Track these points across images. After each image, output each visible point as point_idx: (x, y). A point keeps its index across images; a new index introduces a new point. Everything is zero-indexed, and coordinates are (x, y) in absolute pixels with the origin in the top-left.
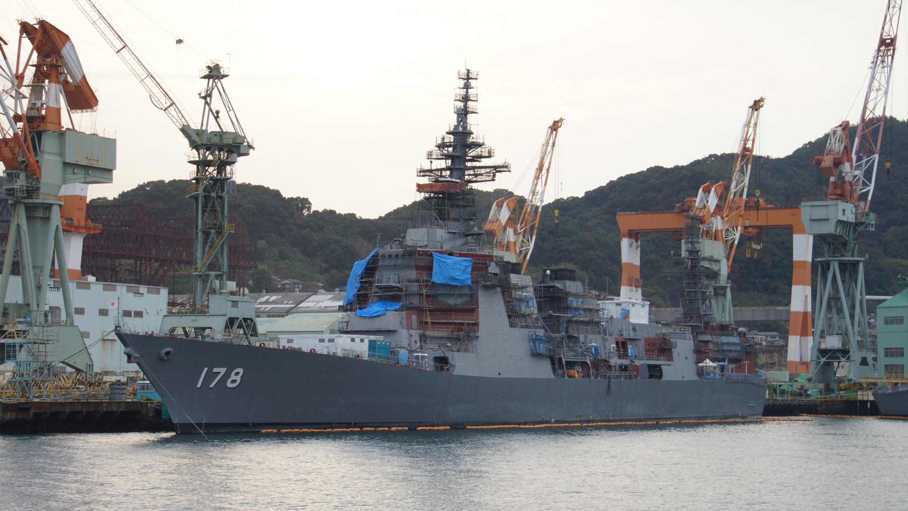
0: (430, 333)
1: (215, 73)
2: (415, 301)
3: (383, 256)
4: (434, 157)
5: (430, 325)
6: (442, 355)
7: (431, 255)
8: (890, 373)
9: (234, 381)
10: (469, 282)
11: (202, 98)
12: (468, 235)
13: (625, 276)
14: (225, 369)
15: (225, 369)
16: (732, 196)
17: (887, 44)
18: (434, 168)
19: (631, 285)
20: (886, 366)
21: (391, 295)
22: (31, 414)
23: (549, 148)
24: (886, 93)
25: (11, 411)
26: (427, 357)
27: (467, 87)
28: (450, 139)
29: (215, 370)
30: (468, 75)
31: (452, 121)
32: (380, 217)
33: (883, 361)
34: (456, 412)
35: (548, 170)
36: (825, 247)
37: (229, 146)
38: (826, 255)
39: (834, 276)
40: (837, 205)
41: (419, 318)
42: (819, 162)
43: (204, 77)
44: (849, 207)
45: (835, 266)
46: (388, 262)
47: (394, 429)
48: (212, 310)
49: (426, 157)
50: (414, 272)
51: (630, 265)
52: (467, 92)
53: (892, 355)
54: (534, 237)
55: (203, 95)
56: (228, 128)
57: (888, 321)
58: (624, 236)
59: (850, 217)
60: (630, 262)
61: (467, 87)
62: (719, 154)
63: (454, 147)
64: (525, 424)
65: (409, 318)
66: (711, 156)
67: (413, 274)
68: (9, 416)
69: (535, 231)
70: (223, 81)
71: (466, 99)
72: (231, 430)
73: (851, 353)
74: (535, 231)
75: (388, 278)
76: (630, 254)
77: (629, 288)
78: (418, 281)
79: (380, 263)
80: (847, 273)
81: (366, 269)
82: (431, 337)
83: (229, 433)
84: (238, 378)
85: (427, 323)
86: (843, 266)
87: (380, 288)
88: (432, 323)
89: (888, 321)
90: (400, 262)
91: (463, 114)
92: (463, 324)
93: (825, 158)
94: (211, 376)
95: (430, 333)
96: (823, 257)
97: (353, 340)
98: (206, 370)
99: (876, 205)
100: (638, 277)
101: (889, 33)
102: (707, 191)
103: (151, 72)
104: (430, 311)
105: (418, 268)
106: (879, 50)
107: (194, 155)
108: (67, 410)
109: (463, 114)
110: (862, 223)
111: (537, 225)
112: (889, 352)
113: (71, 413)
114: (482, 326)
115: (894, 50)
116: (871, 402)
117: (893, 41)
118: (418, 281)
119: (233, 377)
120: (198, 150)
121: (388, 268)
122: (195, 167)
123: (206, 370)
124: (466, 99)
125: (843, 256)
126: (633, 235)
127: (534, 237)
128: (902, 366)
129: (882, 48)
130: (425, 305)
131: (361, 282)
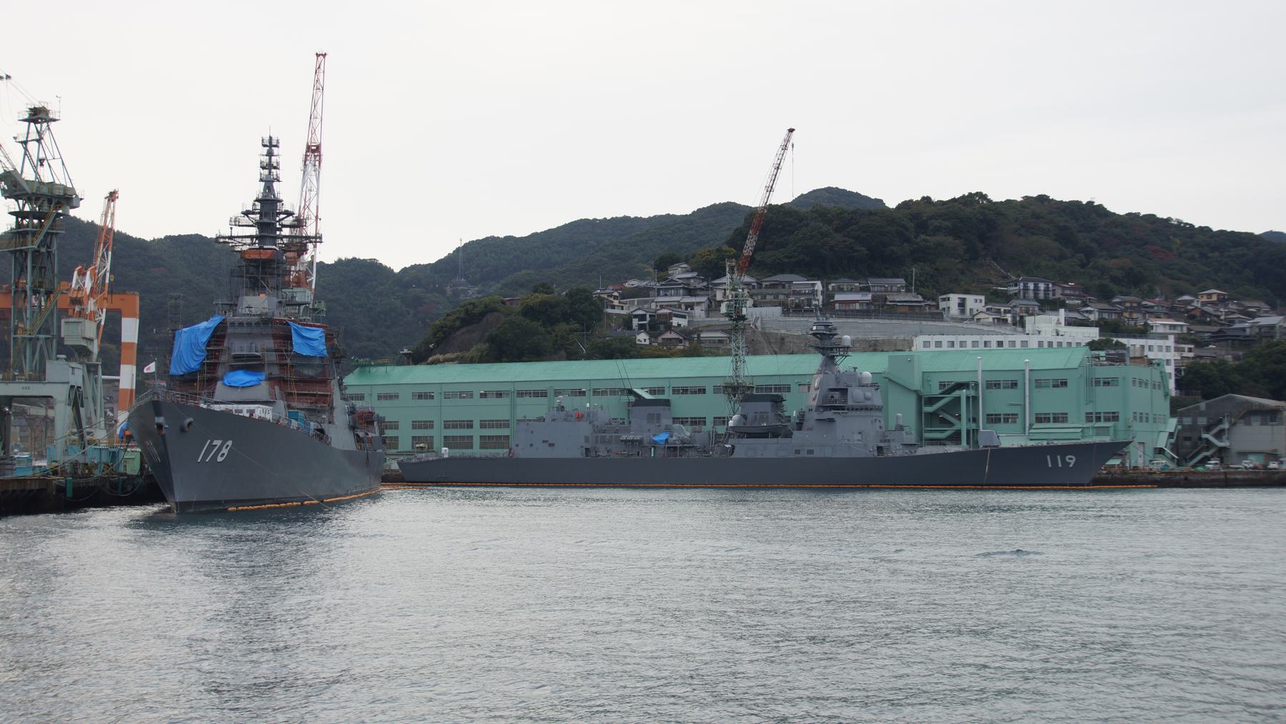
2: (276, 371)
3: (233, 324)
13: (125, 353)
18: (234, 234)
21: (250, 364)
27: (270, 154)
28: (258, 206)
37: (59, 197)
46: (239, 330)
48: (49, 376)
56: (61, 180)
61: (270, 154)
67: (270, 343)
70: (52, 125)
71: (269, 166)
75: (239, 347)
78: (276, 351)
79: (230, 330)
81: (213, 336)
83: (208, 512)
85: (291, 394)
87: (237, 357)
91: (269, 183)
94: (212, 446)
102: (82, 274)
105: (275, 337)
107: (13, 205)
109: (269, 183)
117: (318, 148)
119: (225, 451)
122: (14, 218)
124: (269, 166)
130: (287, 376)
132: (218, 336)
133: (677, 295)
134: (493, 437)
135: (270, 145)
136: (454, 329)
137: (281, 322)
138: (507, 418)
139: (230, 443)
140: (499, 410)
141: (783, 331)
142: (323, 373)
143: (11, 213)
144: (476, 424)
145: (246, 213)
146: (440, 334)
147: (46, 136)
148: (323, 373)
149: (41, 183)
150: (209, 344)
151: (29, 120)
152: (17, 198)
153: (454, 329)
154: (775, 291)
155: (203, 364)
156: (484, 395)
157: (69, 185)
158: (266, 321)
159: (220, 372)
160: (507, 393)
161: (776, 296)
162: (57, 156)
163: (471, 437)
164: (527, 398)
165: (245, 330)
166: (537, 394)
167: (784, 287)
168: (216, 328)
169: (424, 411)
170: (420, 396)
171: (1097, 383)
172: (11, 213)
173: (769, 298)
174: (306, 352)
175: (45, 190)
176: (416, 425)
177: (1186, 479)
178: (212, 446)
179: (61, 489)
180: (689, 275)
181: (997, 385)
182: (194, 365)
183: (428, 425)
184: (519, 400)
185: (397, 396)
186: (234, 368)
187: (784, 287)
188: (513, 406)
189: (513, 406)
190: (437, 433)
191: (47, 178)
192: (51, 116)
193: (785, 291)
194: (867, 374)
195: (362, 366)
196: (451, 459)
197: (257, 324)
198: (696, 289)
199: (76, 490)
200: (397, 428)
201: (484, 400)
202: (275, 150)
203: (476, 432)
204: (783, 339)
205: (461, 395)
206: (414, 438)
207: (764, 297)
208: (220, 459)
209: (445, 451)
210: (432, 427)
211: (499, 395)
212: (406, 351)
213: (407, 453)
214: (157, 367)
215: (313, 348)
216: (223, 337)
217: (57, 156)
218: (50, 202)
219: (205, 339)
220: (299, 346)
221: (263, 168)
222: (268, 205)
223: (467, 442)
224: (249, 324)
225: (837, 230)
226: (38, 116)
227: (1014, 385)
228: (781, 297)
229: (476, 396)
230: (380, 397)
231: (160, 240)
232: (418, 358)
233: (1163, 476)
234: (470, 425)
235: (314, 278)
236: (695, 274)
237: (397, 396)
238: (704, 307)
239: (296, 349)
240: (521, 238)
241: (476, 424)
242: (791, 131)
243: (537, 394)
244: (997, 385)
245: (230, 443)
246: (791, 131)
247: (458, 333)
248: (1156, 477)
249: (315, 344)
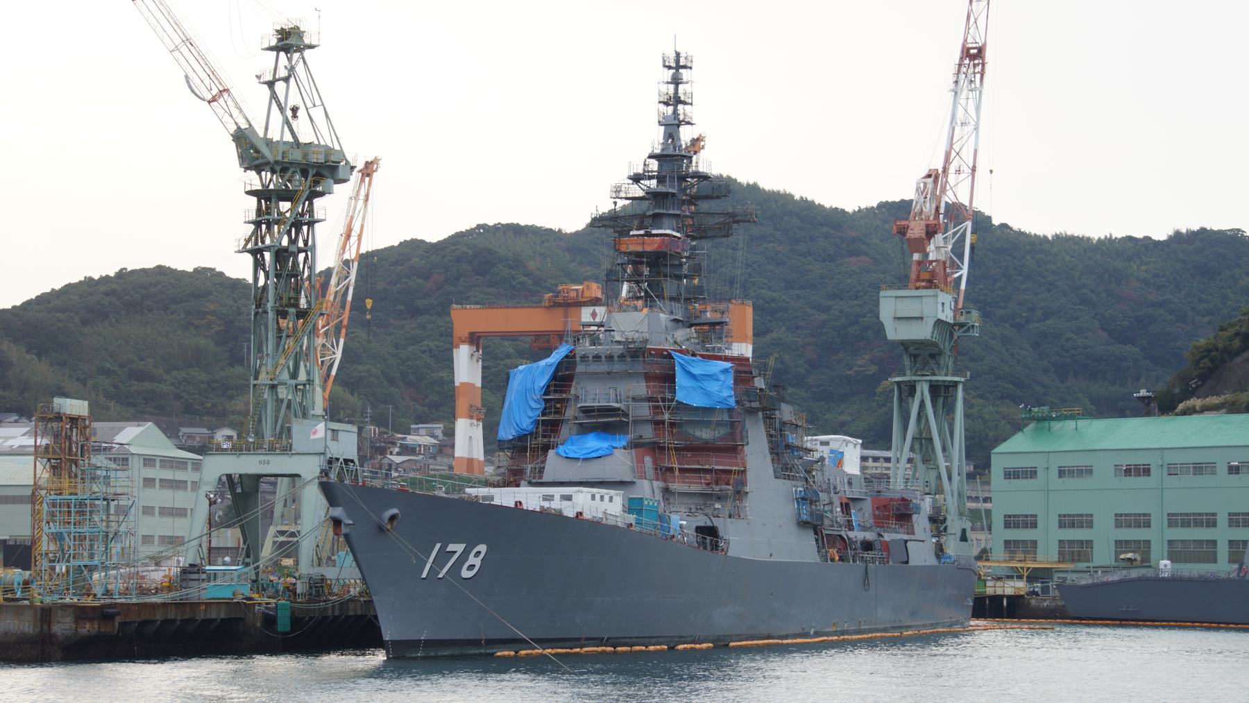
0: (676, 486)
1: (292, 41)
2: (648, 433)
3: (584, 358)
4: (622, 195)
5: (677, 473)
6: (709, 524)
7: (670, 356)
8: (1014, 552)
9: (471, 567)
10: (732, 402)
11: (226, 90)
12: (692, 325)
13: (462, 404)
14: (463, 546)
15: (463, 546)
16: (332, 298)
17: (974, 55)
19: (471, 417)
20: (1007, 543)
21: (606, 422)
22: (117, 625)
23: (361, 203)
24: (976, 129)
25: (91, 620)
26: (682, 522)
27: (676, 81)
28: (654, 165)
29: (451, 547)
30: (677, 61)
31: (654, 138)
32: (14, 307)
33: (1001, 534)
34: (722, 619)
35: (360, 237)
36: (907, 361)
37: (319, 166)
38: (908, 372)
39: (922, 405)
40: (936, 296)
41: (655, 462)
42: (903, 231)
43: (271, 49)
44: (946, 298)
45: (923, 389)
46: (594, 368)
47: (652, 648)
49: (608, 194)
50: (643, 384)
51: (468, 386)
52: (676, 90)
53: (1072, 525)
54: (342, 341)
55: (269, 78)
57: (1011, 474)
58: (463, 342)
59: (947, 316)
60: (471, 381)
61: (676, 81)
62: (491, 224)
63: (661, 179)
64: (786, 637)
65: (640, 461)
66: (479, 226)
68: (87, 629)
69: (343, 331)
70: (307, 53)
71: (675, 101)
72: (457, 651)
73: (948, 522)
74: (343, 331)
75: (591, 393)
76: (466, 368)
77: (469, 421)
78: (649, 399)
79: (580, 368)
80: (941, 401)
81: (554, 377)
82: (681, 494)
84: (477, 562)
85: (671, 470)
86: (935, 389)
87: (587, 411)
88: (680, 469)
89: (1011, 474)
90: (618, 367)
92: (729, 472)
93: (912, 224)
94: (444, 555)
95: (676, 486)
96: (904, 375)
97: (593, 497)
98: (438, 546)
99: (973, 298)
100: (479, 405)
101: (975, 39)
103: (190, 34)
104: (676, 449)
105: (648, 377)
106: (960, 65)
107: (254, 180)
108: (159, 617)
109: (672, 126)
110: (962, 325)
111: (345, 322)
112: (1011, 522)
113: (163, 622)
114: (750, 476)
115: (983, 65)
116: (1009, 597)
118: (649, 399)
119: (472, 560)
120: (259, 173)
121: (595, 376)
123: (438, 546)
124: (675, 101)
125: (934, 374)
126: (474, 339)
127: (342, 341)
128: (1035, 543)
129: (967, 61)
130: (666, 439)
131: (545, 400)
132: (562, 379)
135: (677, 67)
136: (1230, 354)
137: (660, 353)
139: (483, 548)
142: (732, 435)
143: (251, 193)
144: (1222, 520)
145: (636, 179)
146: (1206, 362)
147: (300, 69)
148: (732, 435)
149: (297, 143)
151: (276, 49)
152: (258, 169)
153: (1230, 354)
155: (537, 422)
157: (337, 148)
158: (635, 352)
162: (318, 102)
163: (1214, 543)
165: (603, 367)
168: (559, 366)
169: (1136, 496)
170: (1128, 472)
172: (251, 193)
174: (697, 401)
175: (296, 156)
176: (1123, 520)
178: (444, 555)
179: (270, 620)
183: (1143, 521)
185: (1088, 471)
186: (584, 430)
190: (1158, 535)
191: (306, 136)
192: (307, 41)
195: (1040, 420)
196: (1175, 580)
197: (622, 357)
199: (296, 621)
200: (1090, 525)
203: (1223, 534)
205: (1199, 469)
206: (1119, 543)
208: (466, 574)
209: (1165, 564)
212: (1143, 393)
213: (1106, 569)
215: (708, 394)
217: (318, 102)
218: (304, 173)
219: (543, 382)
220: (686, 392)
221: (667, 104)
222: (673, 160)
223: (1206, 551)
224: (610, 358)
229: (1222, 469)
230: (1062, 473)
231: (870, 210)
232: (1166, 405)
235: (964, 271)
237: (1088, 471)
239: (680, 396)
240: (439, 243)
241: (1222, 520)
245: (483, 548)
247: (1239, 360)
249: (713, 387)
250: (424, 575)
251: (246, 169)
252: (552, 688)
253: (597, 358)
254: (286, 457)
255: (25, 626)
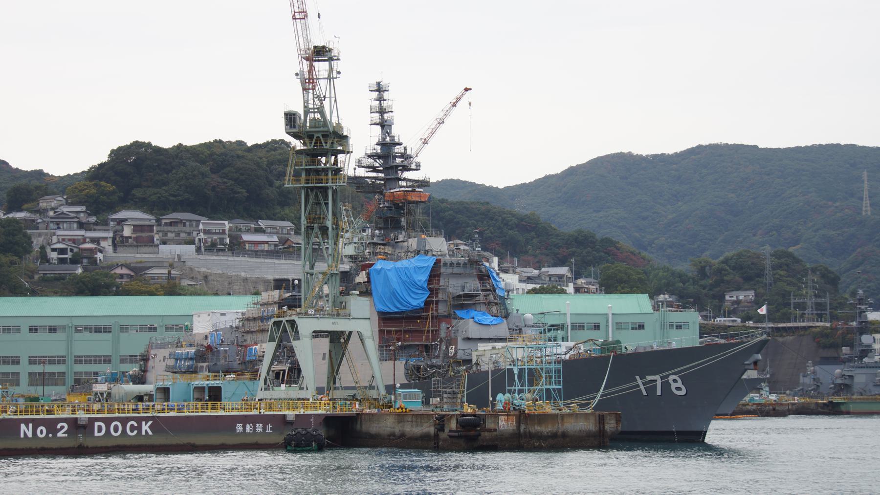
3: (445, 264)
27: (380, 99)
28: (378, 148)
61: (380, 99)
79: (443, 270)
91: (385, 125)
121: (453, 275)
124: (382, 111)
133: (70, 229)
134: (54, 373)
135: (380, 89)
138: (62, 353)
140: (53, 345)
141: (203, 270)
144: (24, 361)
150: (430, 281)
154: (176, 229)
156: (33, 330)
159: (442, 309)
160: (64, 328)
161: (178, 234)
164: (87, 334)
165: (456, 270)
166: (98, 330)
167: (185, 225)
171: (671, 326)
173: (171, 235)
177: (774, 409)
180: (78, 209)
181: (581, 327)
182: (417, 301)
184: (77, 336)
187: (185, 225)
188: (70, 343)
189: (70, 343)
193: (187, 229)
194: (528, 315)
197: (465, 264)
198: (89, 223)
201: (34, 335)
202: (386, 95)
203: (24, 369)
204: (206, 277)
207: (166, 234)
210: (18, 363)
211: (52, 330)
214: (768, 310)
216: (439, 276)
219: (422, 278)
224: (458, 264)
225: (214, 171)
226: (320, 53)
227: (597, 327)
228: (183, 235)
229: (25, 330)
233: (754, 407)
234: (16, 361)
236: (84, 208)
238: (110, 242)
241: (24, 361)
242: (466, 90)
243: (98, 330)
244: (581, 327)
246: (466, 90)
248: (749, 407)
250: (659, 393)
251: (346, 137)
252: (643, 454)
253: (452, 264)
254: (347, 320)
255: (429, 428)
